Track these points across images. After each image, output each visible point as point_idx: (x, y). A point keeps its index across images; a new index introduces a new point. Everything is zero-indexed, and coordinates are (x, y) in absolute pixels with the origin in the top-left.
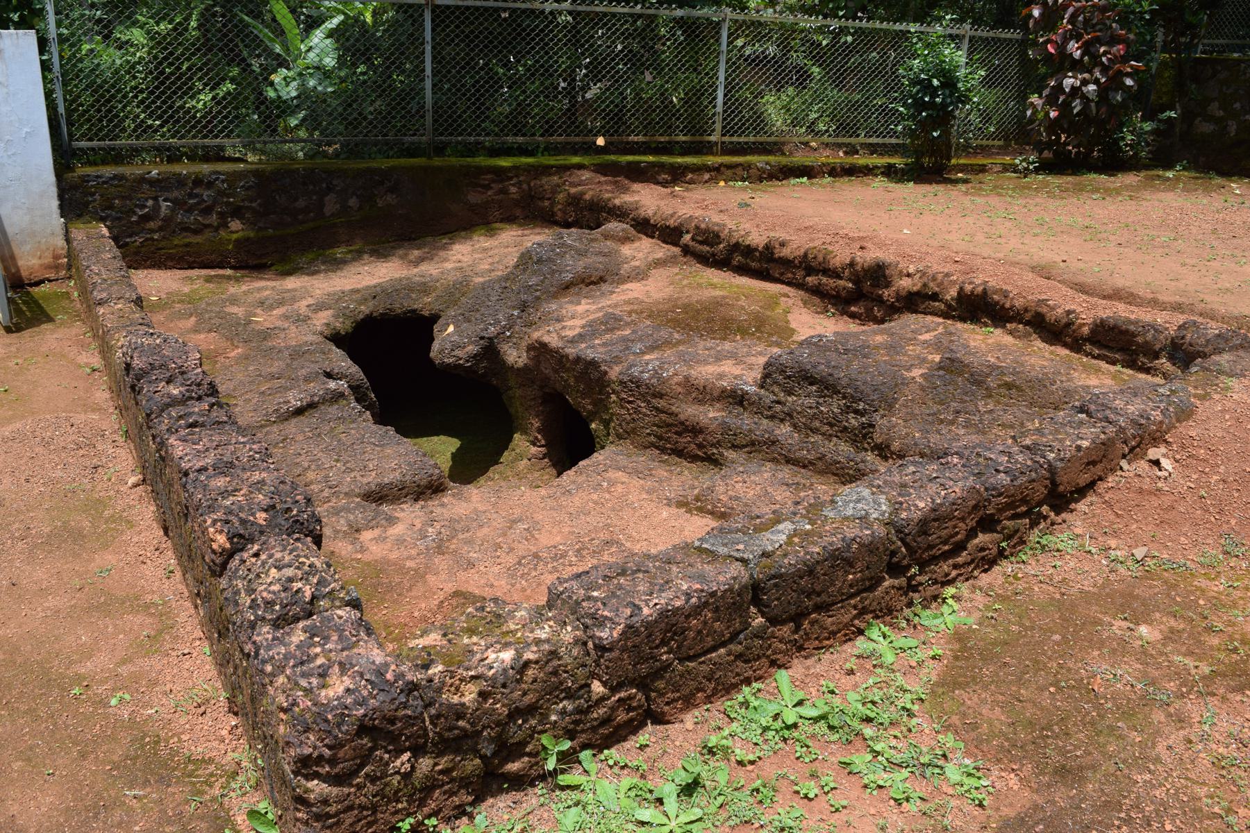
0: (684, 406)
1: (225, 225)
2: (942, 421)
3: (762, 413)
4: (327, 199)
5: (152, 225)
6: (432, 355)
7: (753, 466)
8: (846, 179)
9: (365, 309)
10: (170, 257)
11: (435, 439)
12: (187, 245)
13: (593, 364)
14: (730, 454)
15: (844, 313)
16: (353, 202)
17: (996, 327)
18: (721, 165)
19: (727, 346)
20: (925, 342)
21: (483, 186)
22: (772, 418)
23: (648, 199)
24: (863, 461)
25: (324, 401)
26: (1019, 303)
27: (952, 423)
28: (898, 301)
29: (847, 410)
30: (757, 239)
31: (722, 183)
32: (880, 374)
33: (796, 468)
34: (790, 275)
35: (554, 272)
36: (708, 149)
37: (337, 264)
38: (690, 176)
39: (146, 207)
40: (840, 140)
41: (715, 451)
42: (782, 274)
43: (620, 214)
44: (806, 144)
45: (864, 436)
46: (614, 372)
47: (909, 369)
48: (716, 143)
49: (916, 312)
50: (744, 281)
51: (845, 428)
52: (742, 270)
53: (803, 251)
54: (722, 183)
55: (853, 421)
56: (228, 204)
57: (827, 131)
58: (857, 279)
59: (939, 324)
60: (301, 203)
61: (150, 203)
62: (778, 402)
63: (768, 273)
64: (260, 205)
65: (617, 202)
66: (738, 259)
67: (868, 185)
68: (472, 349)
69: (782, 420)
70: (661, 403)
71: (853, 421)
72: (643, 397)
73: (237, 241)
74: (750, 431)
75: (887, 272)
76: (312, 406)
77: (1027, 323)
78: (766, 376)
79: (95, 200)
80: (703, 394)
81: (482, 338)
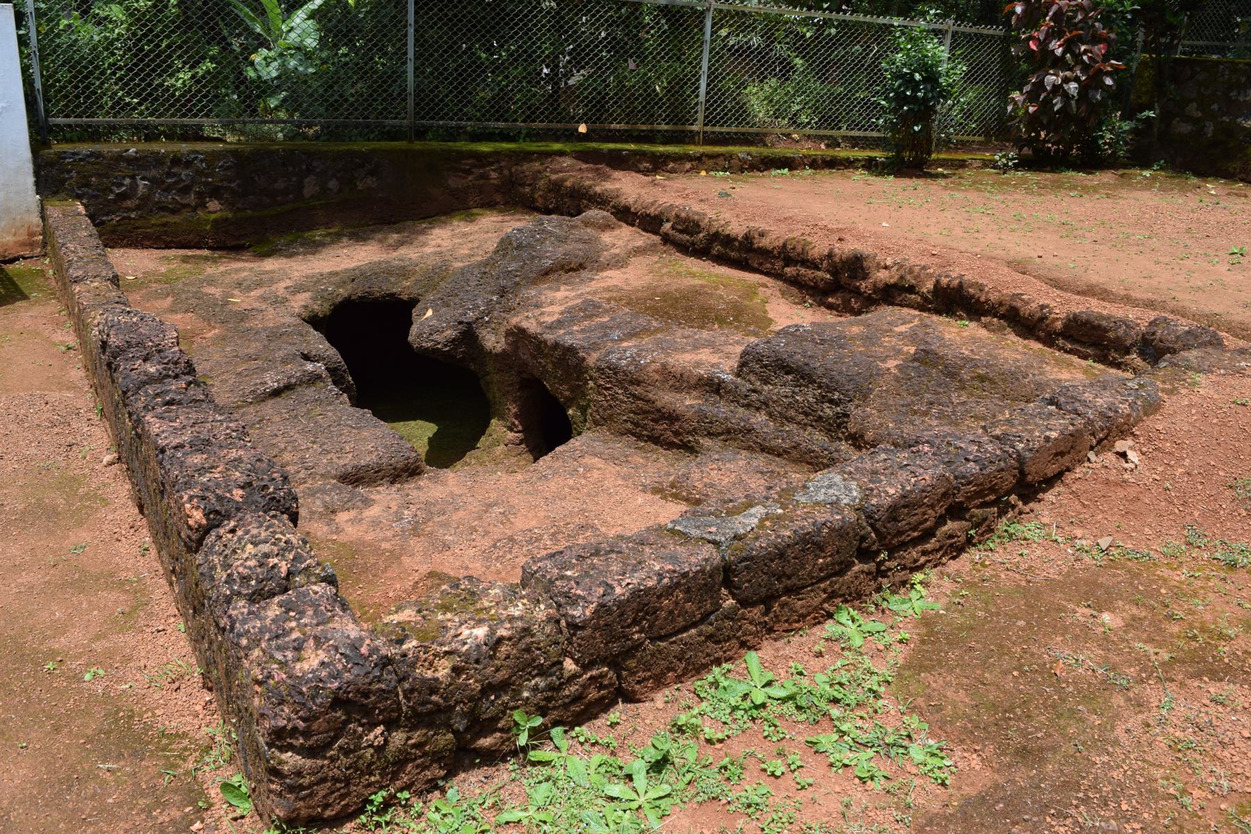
0: (660, 393)
1: (203, 205)
2: (915, 412)
3: (738, 402)
4: (307, 180)
5: (129, 203)
6: (410, 339)
7: (728, 454)
8: (827, 171)
9: (343, 292)
10: (147, 237)
11: (412, 423)
12: (164, 225)
13: (571, 350)
14: (706, 442)
15: (821, 303)
16: (333, 184)
17: (971, 320)
18: (703, 155)
19: (705, 334)
20: (901, 334)
21: (464, 171)
22: (748, 406)
23: (629, 187)
24: (837, 451)
25: (301, 383)
26: (994, 297)
27: (925, 414)
28: (875, 292)
29: (822, 399)
30: (737, 228)
31: (703, 173)
32: (856, 365)
33: (770, 457)
34: (769, 266)
35: (533, 258)
36: (649, 138)
37: (314, 247)
38: (672, 165)
39: (121, 185)
40: (822, 132)
41: (691, 438)
42: (761, 264)
43: (601, 201)
44: (788, 135)
45: (839, 426)
46: (592, 359)
47: (884, 360)
48: (698, 133)
49: (892, 304)
50: (723, 270)
51: (820, 418)
52: (721, 260)
53: (782, 241)
54: (703, 173)
55: (828, 411)
56: (206, 183)
57: (809, 123)
58: (835, 270)
59: (915, 316)
60: (280, 185)
61: (127, 181)
62: (754, 391)
63: (747, 263)
64: (239, 185)
65: (598, 189)
66: (717, 248)
67: (849, 178)
68: (451, 333)
69: (758, 409)
70: (638, 390)
71: (828, 411)
72: (620, 384)
73: (215, 221)
74: (726, 418)
75: (865, 264)
76: (289, 387)
77: (1002, 317)
78: (743, 365)
79: (71, 178)
80: (679, 381)
81: (460, 323)
